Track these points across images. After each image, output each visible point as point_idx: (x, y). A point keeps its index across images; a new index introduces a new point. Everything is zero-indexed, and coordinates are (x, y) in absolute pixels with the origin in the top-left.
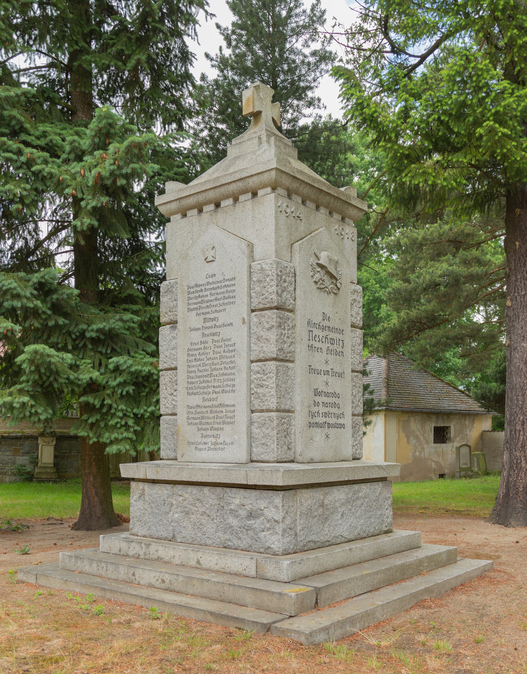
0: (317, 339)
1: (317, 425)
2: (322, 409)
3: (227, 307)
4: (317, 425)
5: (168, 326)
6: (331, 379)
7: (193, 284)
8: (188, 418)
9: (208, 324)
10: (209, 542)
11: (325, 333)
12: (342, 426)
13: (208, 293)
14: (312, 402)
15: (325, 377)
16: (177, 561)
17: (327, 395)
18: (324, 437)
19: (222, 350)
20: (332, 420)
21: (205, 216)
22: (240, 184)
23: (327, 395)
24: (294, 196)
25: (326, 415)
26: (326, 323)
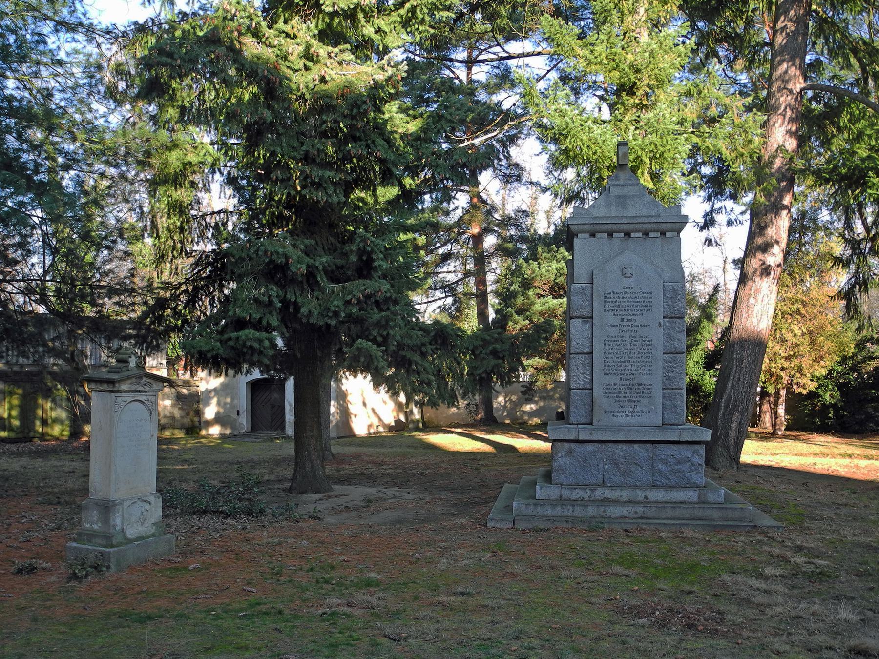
3: (644, 313)
5: (580, 320)
7: (610, 291)
8: (605, 393)
9: (625, 323)
10: (639, 484)
13: (626, 300)
16: (624, 499)
19: (639, 343)
21: (616, 242)
22: (672, 225)
24: (598, 235)
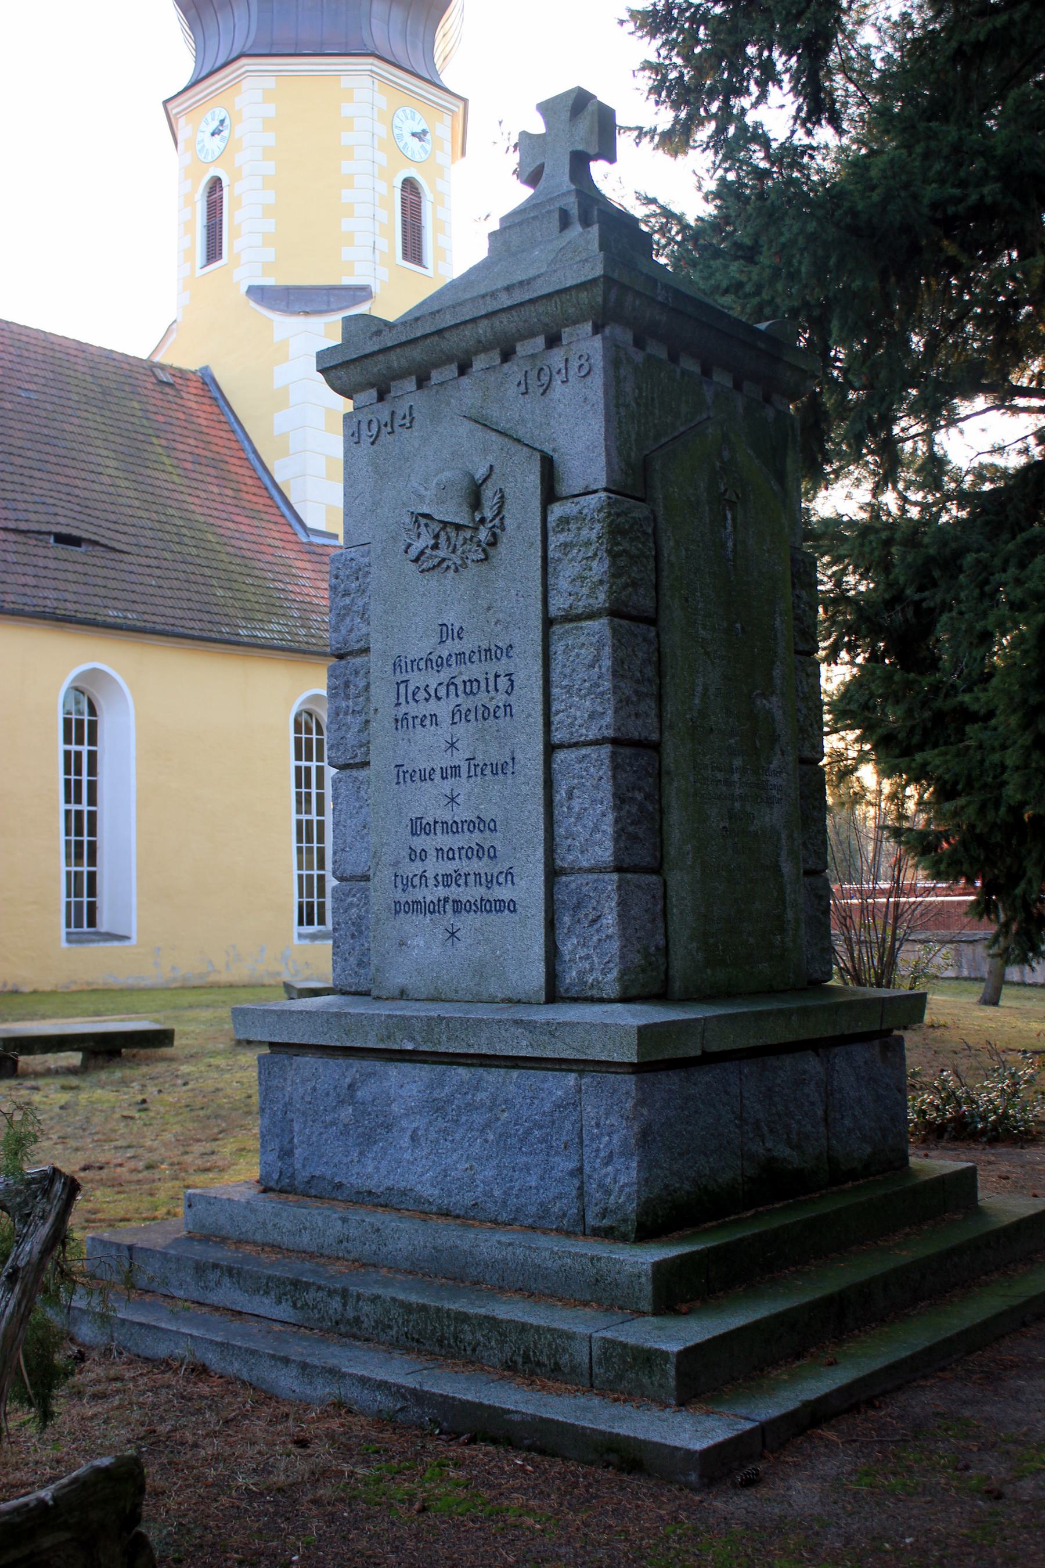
0: (422, 695)
1: (417, 907)
2: (434, 867)
4: (417, 907)
6: (463, 786)
11: (445, 676)
12: (511, 906)
14: (405, 853)
15: (446, 786)
17: (452, 828)
18: (441, 935)
20: (472, 893)
23: (452, 828)
25: (447, 880)
26: (452, 646)
